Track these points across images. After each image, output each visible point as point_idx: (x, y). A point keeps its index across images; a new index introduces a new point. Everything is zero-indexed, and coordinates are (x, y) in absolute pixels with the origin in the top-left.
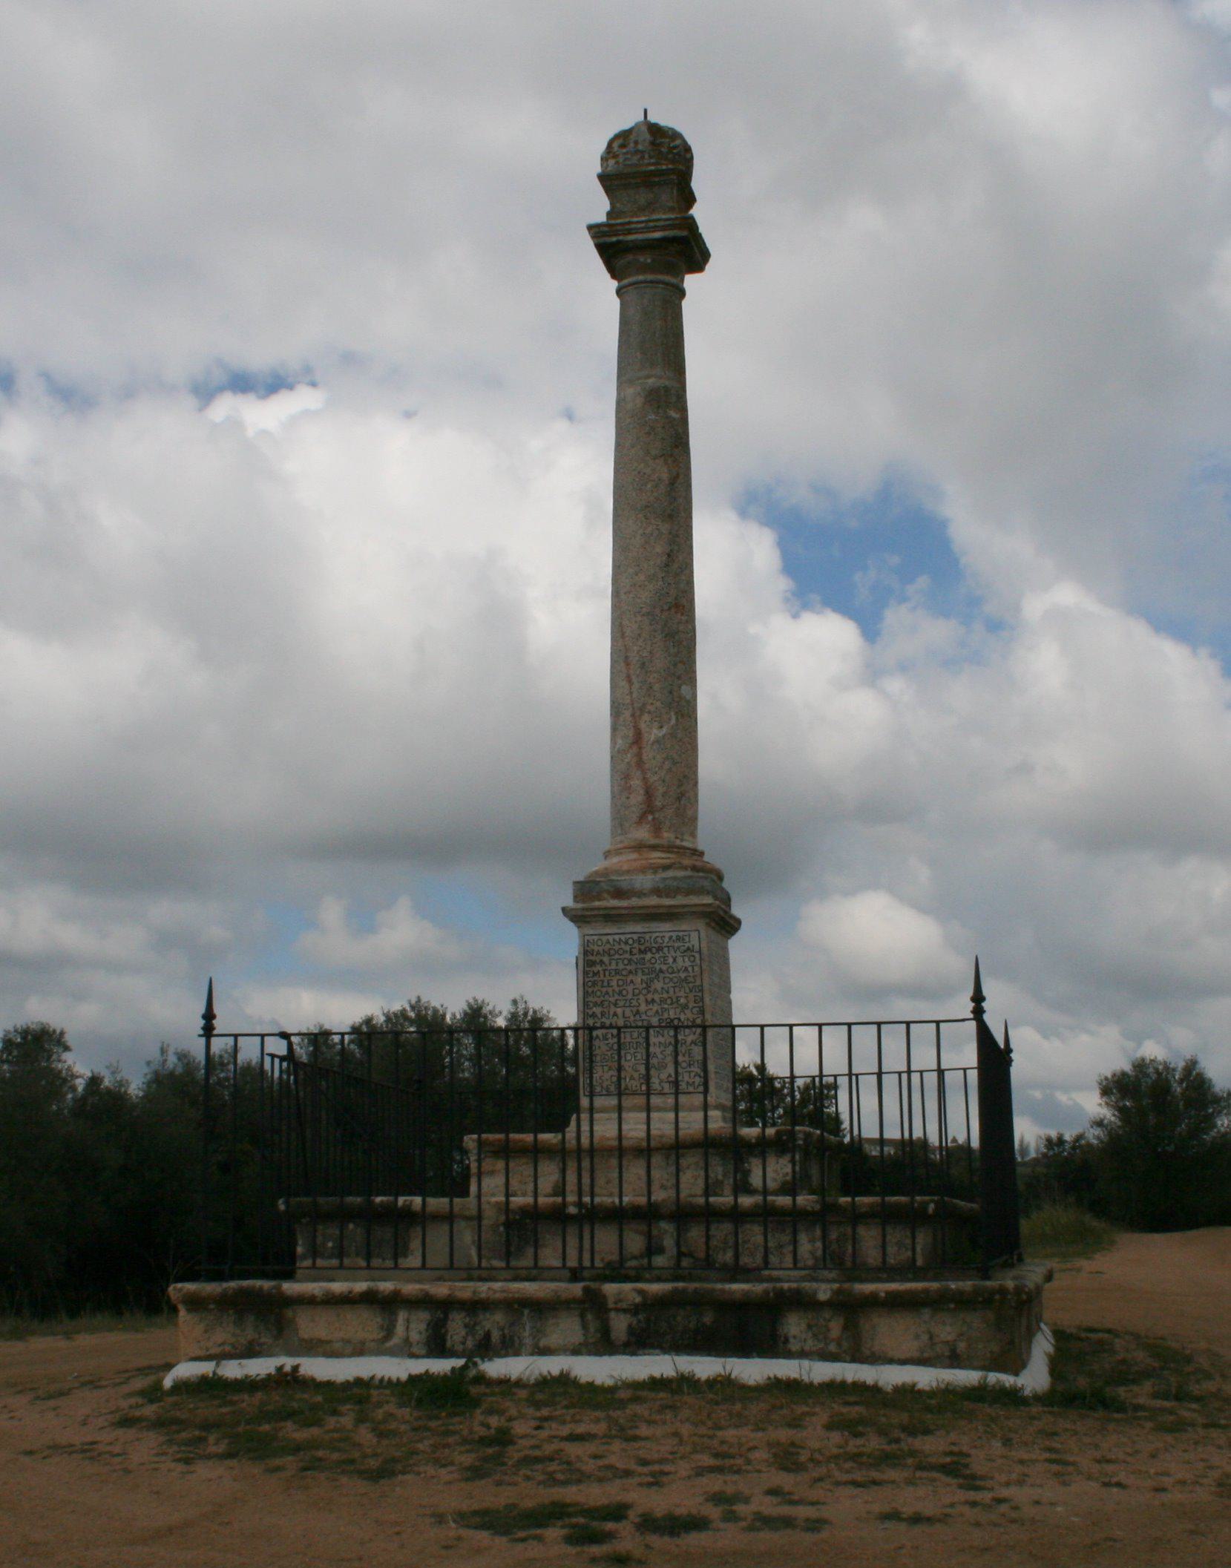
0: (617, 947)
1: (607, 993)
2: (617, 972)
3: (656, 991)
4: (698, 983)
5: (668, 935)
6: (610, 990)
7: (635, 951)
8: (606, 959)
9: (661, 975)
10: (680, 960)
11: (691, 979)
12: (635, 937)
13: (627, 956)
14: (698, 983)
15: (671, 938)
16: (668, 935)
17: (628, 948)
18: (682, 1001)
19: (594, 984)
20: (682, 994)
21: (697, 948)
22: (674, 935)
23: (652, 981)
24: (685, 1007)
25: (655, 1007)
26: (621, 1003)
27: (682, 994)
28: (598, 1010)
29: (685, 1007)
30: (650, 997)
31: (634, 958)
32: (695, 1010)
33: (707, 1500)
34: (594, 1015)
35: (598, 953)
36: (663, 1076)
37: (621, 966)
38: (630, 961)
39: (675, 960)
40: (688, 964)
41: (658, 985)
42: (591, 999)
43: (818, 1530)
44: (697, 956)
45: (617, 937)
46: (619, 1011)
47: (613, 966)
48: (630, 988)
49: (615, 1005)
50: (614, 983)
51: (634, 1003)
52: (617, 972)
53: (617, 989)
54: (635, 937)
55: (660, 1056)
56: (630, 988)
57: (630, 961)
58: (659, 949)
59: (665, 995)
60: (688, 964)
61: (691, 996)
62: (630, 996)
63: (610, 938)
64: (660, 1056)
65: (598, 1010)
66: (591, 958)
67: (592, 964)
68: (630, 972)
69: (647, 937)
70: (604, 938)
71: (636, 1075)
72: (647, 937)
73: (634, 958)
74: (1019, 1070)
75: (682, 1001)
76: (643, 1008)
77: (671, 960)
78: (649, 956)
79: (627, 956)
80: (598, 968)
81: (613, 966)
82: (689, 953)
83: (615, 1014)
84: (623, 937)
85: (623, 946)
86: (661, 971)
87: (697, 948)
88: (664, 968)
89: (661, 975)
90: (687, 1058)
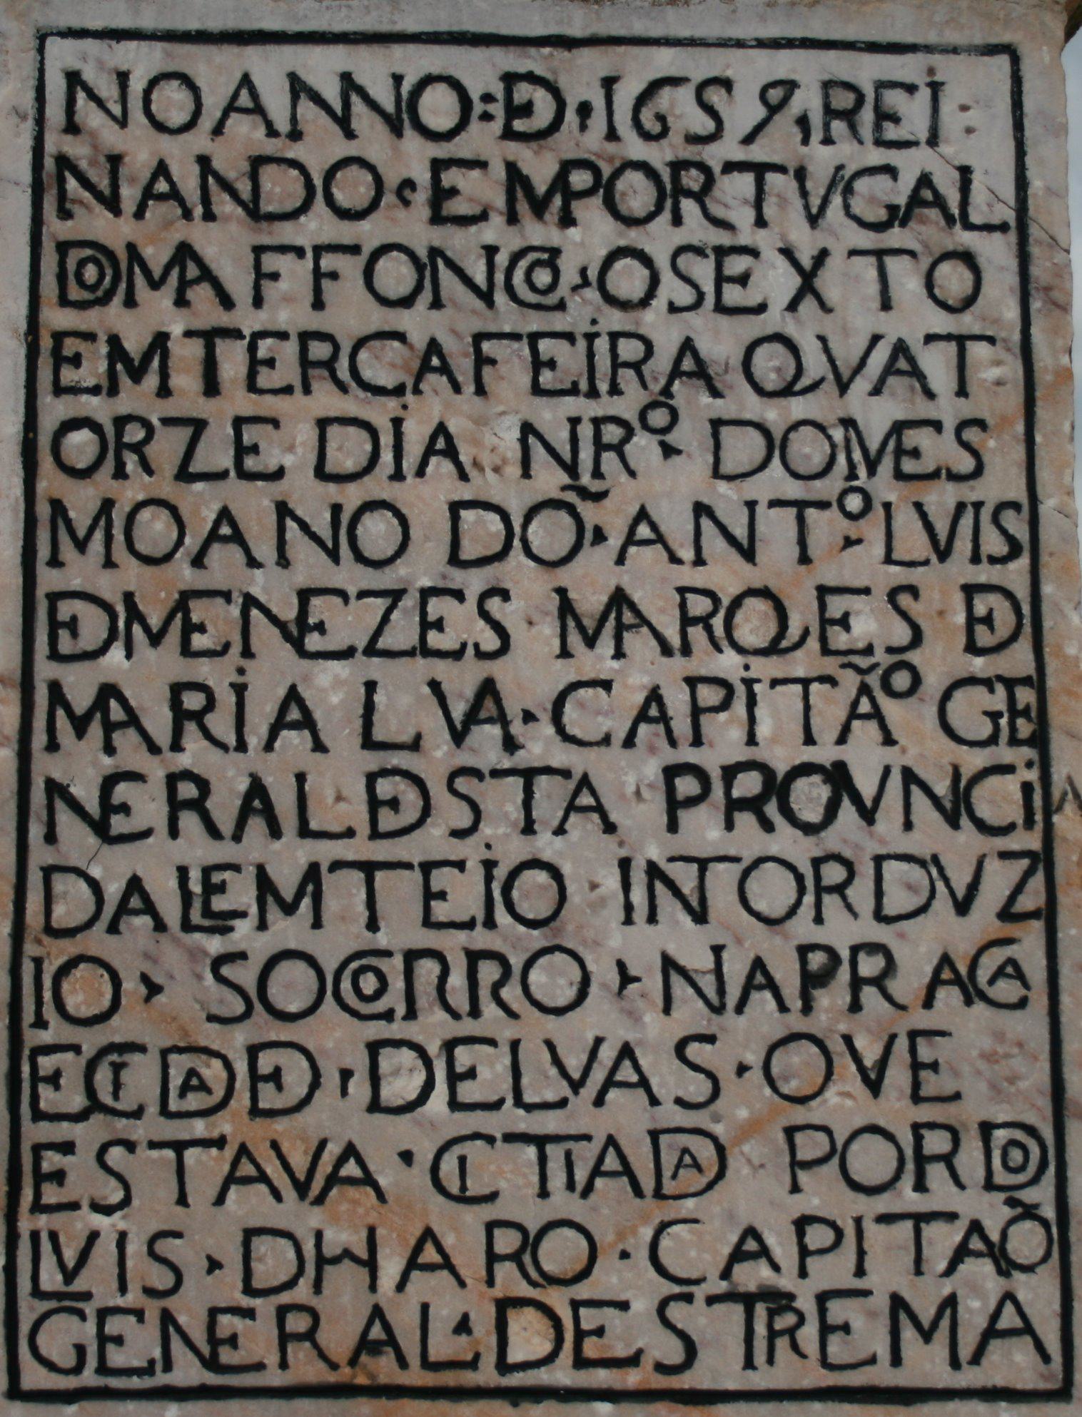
0: (321, 147)
1: (226, 528)
2: (321, 359)
3: (643, 528)
4: (1002, 481)
5: (749, 71)
6: (255, 507)
7: (479, 189)
8: (224, 245)
9: (695, 405)
10: (850, 283)
11: (938, 449)
12: (480, 71)
13: (413, 226)
14: (1002, 481)
15: (777, 95)
16: (749, 71)
17: (412, 158)
18: (870, 624)
19: (120, 446)
20: (865, 565)
21: (992, 195)
22: (809, 70)
23: (612, 440)
24: (895, 674)
25: (641, 669)
26: (347, 624)
27: (865, 565)
28: (145, 675)
29: (895, 674)
30: (591, 581)
31: (463, 244)
32: (969, 711)
33: (251, 775)
34: (109, 712)
35: (159, 187)
36: (698, 1250)
37: (351, 312)
38: (429, 265)
39: (808, 286)
40: (916, 317)
41: (667, 484)
42: (80, 571)
43: (226, 930)
44: (996, 253)
45: (322, 66)
46: (331, 689)
47: (288, 308)
48: (428, 496)
49: (296, 633)
50: (289, 449)
51: (461, 624)
52: (321, 359)
53: (313, 501)
54: (480, 71)
55: (669, 1079)
56: (428, 496)
57: (429, 265)
58: (678, 187)
59: (726, 573)
60: (916, 317)
61: (941, 590)
62: (423, 567)
63: (269, 69)
64: (669, 1079)
65: (145, 675)
66: (97, 224)
67: (118, 274)
68: (432, 359)
69: (580, 76)
70: (216, 71)
71: (463, 1233)
72: (580, 76)
73: (463, 244)
74: (951, 1182)
75: (870, 624)
76: (531, 673)
77: (776, 281)
78: (592, 234)
79: (413, 226)
80: (159, 311)
81: (288, 308)
82: (927, 232)
83: (295, 712)
84: (374, 70)
85: (372, 139)
86: (692, 365)
87: (992, 195)
88: (720, 342)
89: (695, 405)
90: (895, 1109)
